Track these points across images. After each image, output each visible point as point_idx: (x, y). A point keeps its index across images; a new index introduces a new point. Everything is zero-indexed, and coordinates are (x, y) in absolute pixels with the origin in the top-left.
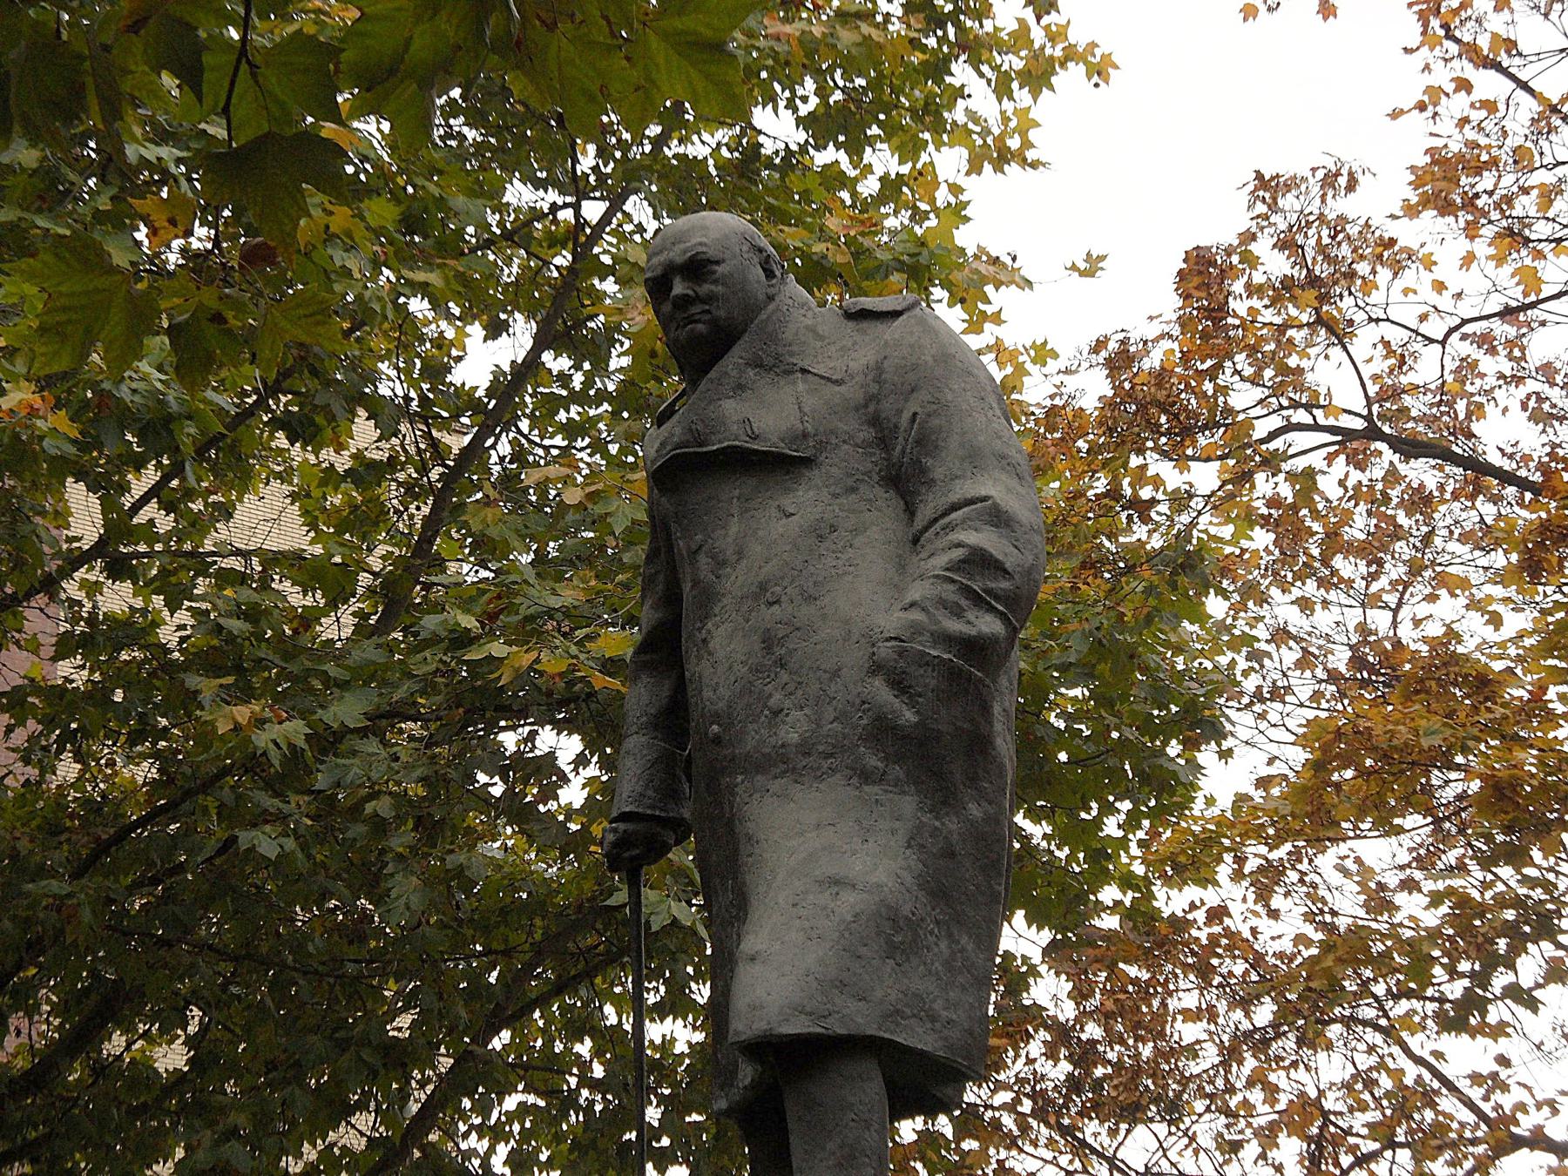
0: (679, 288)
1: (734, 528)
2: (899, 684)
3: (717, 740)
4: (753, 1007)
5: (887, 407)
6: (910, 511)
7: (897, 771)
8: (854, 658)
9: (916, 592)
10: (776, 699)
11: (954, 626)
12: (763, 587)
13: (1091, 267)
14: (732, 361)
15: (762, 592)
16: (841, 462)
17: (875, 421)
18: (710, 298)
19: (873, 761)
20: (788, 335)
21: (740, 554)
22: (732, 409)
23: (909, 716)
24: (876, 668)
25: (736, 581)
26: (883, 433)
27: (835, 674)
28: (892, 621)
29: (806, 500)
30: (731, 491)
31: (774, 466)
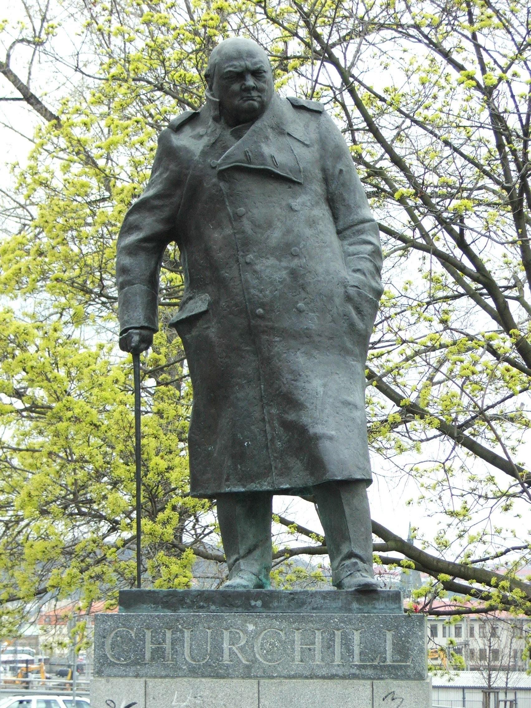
3: (261, 317)
5: (329, 163)
6: (335, 218)
10: (301, 305)
16: (317, 188)
19: (349, 345)
24: (348, 298)
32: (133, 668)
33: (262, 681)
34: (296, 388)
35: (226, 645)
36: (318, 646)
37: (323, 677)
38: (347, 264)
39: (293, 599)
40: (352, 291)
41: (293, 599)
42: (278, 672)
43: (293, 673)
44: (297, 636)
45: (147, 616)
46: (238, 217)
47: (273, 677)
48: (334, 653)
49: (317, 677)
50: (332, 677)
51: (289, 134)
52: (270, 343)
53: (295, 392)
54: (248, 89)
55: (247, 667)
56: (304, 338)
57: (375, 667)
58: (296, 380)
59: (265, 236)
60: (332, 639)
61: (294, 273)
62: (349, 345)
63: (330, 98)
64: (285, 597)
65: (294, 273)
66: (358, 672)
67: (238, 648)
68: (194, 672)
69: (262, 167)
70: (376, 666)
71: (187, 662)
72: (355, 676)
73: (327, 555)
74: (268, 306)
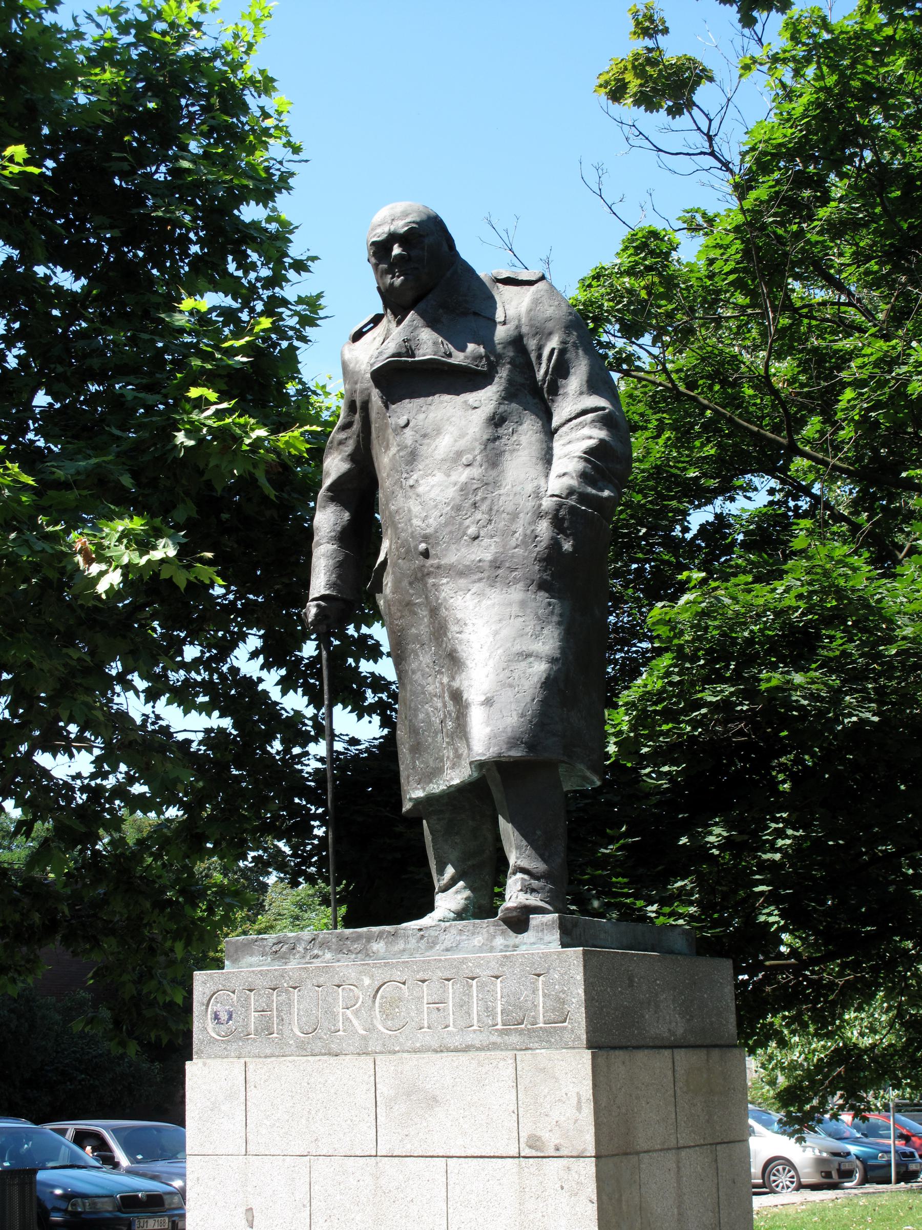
32: (235, 1046)
33: (379, 1058)
34: (461, 642)
37: (456, 1050)
39: (422, 937)
41: (422, 937)
42: (401, 1044)
43: (418, 1045)
45: (250, 972)
47: (395, 1052)
48: (469, 1014)
49: (449, 1050)
50: (467, 1049)
51: (476, 314)
53: (459, 648)
55: (364, 1038)
57: (521, 1032)
58: (460, 633)
59: (433, 447)
64: (413, 935)
66: (499, 1040)
67: (353, 1012)
68: (303, 1049)
69: (746, 424)
70: (522, 1030)
71: (295, 1035)
72: (494, 1046)
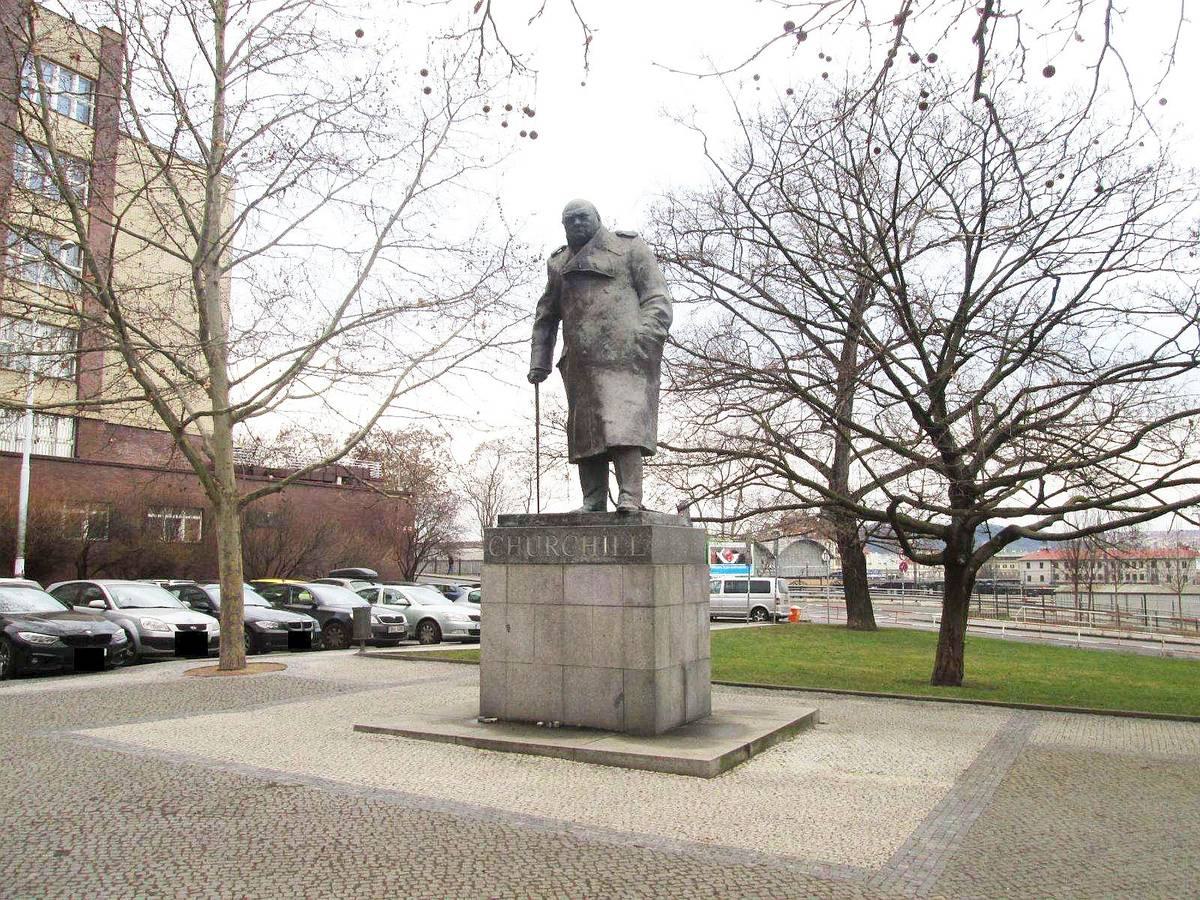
0: (578, 222)
1: (589, 295)
2: (643, 347)
3: (585, 356)
4: (614, 436)
5: (634, 265)
6: (639, 296)
7: (642, 372)
8: (631, 338)
9: (647, 320)
10: (607, 346)
11: (657, 332)
12: (601, 313)
13: (505, 125)
14: (589, 245)
15: (601, 315)
16: (625, 279)
17: (631, 268)
18: (586, 226)
19: (635, 368)
20: (604, 239)
21: (592, 302)
22: (590, 259)
23: (646, 356)
24: (637, 341)
25: (592, 309)
26: (633, 273)
27: (625, 342)
28: (640, 328)
29: (613, 290)
30: (591, 282)
31: (603, 278)
35: (547, 546)
36: (595, 545)
38: (640, 320)
40: (639, 337)
44: (584, 539)
46: (575, 300)
52: (591, 371)
54: (579, 226)
56: (609, 366)
60: (602, 540)
61: (604, 329)
62: (635, 368)
63: (407, 256)
65: (604, 329)
72: (614, 563)
73: (943, 567)
74: (589, 350)
